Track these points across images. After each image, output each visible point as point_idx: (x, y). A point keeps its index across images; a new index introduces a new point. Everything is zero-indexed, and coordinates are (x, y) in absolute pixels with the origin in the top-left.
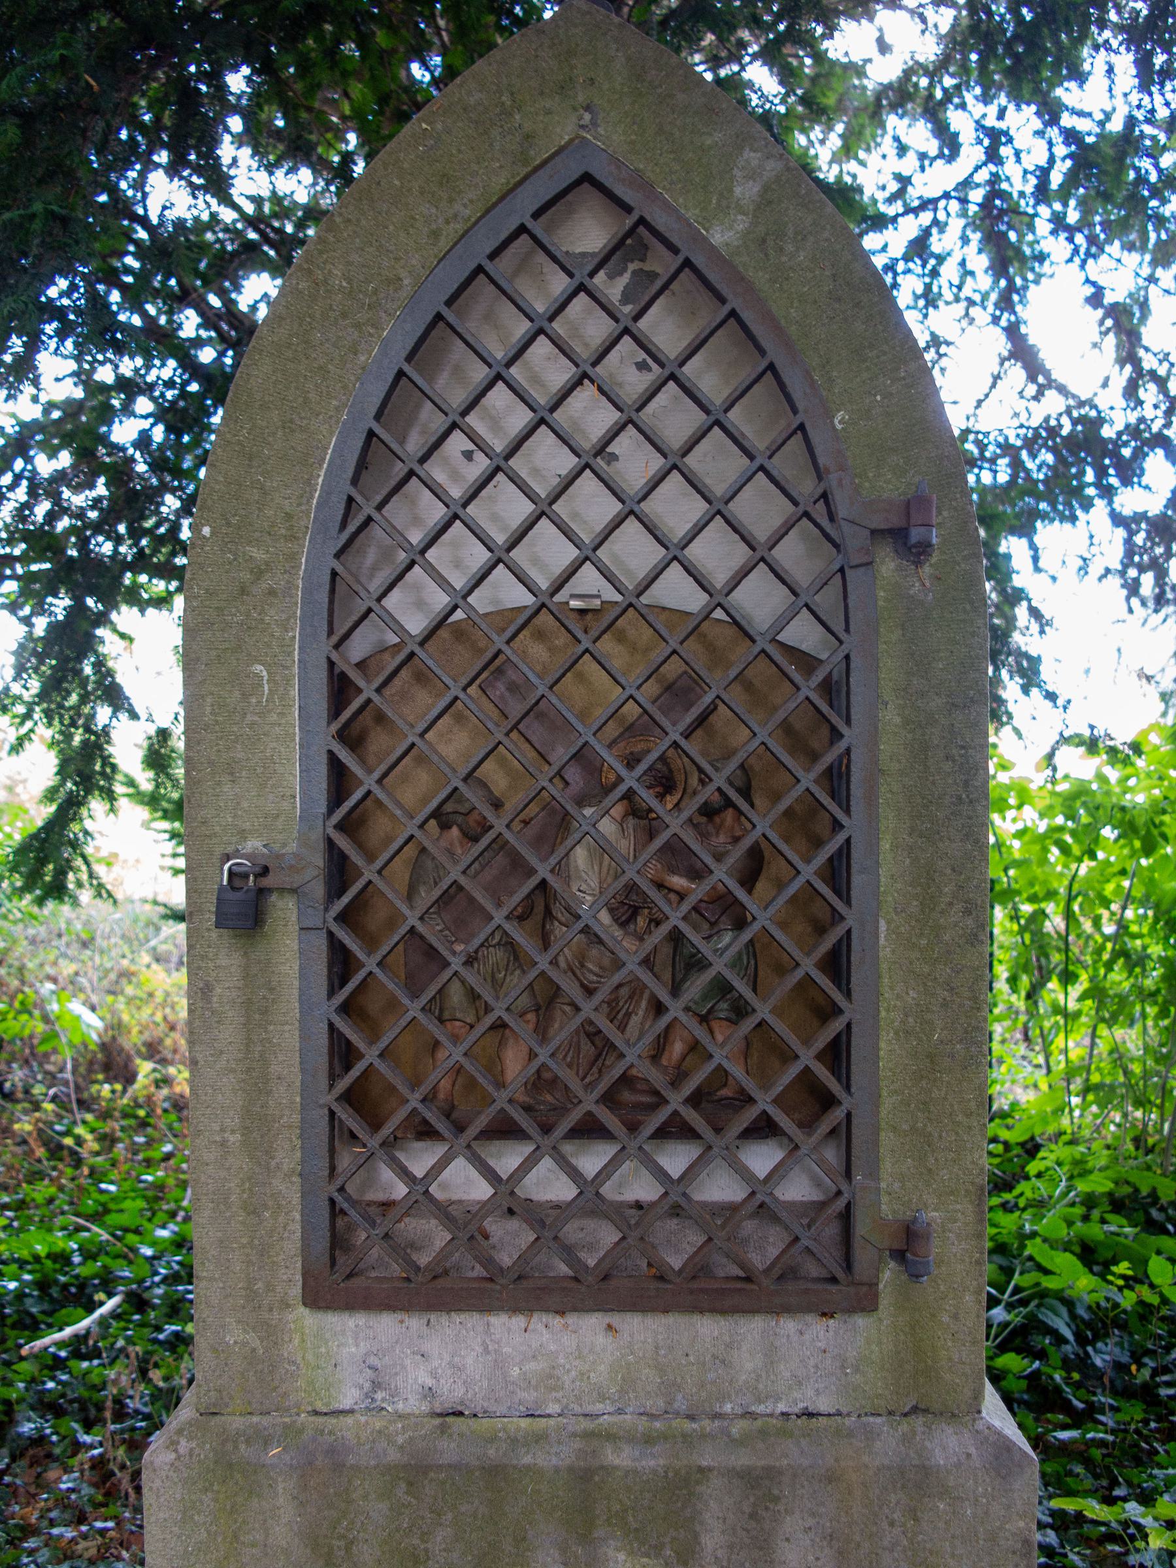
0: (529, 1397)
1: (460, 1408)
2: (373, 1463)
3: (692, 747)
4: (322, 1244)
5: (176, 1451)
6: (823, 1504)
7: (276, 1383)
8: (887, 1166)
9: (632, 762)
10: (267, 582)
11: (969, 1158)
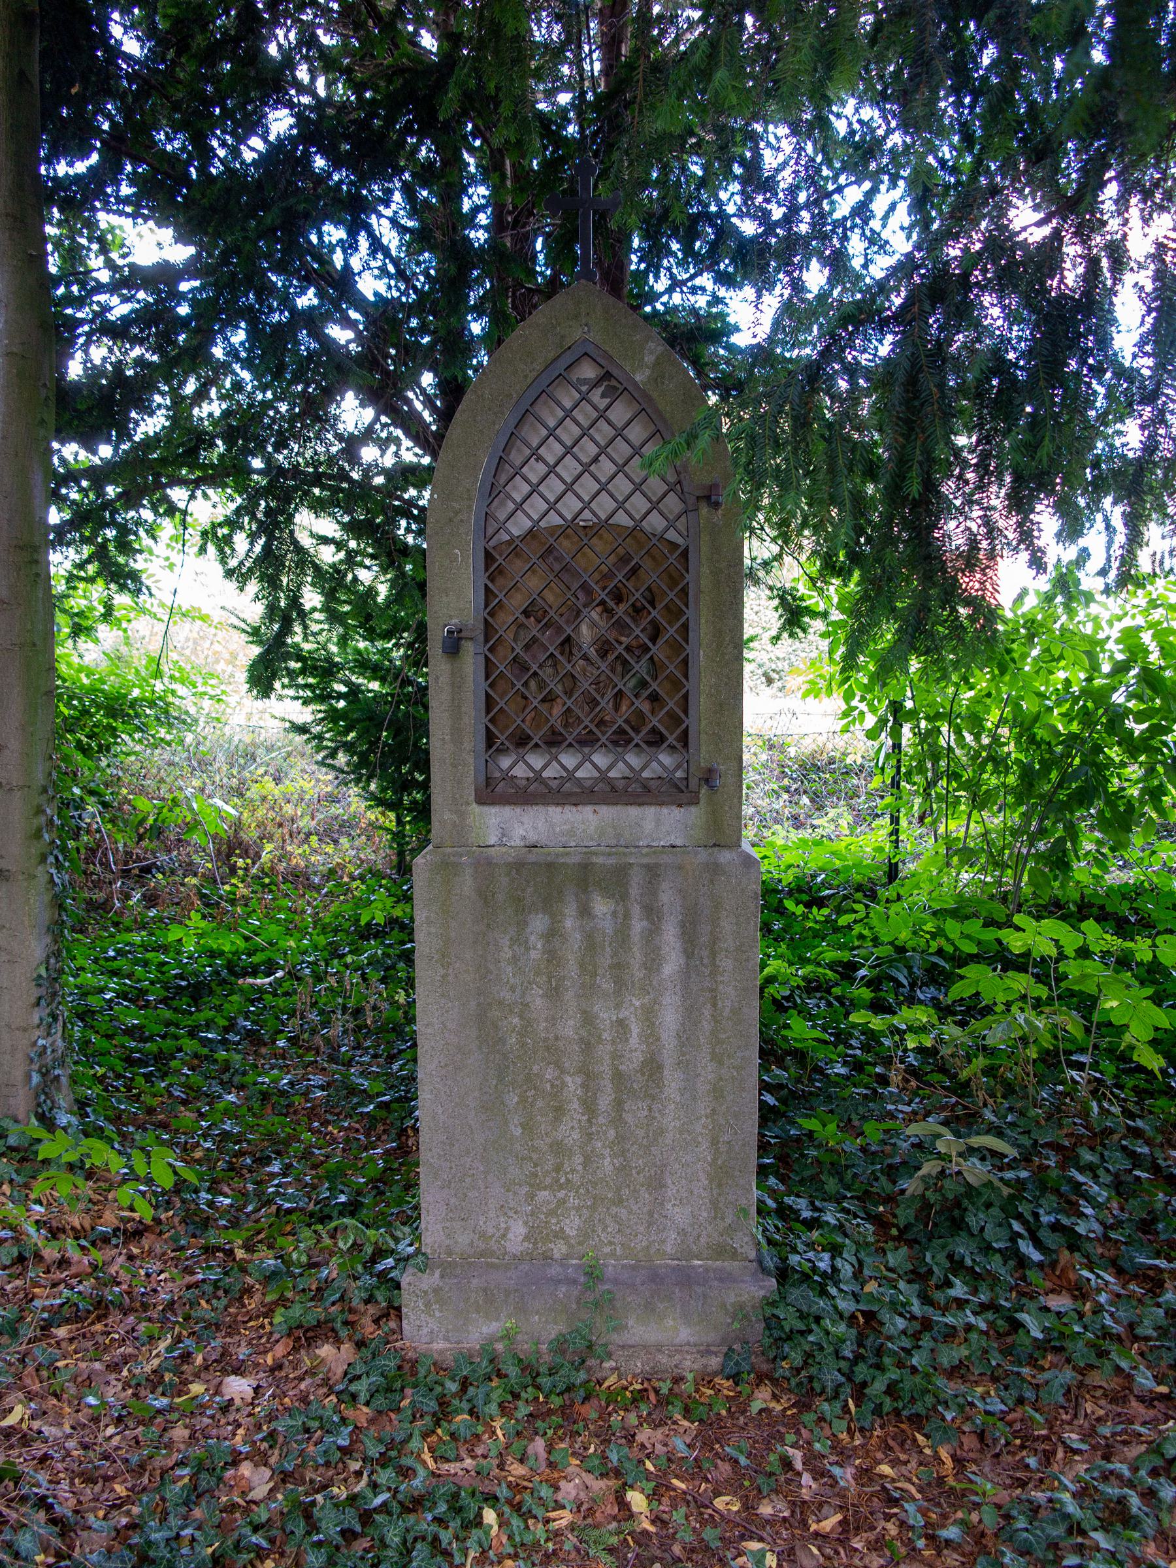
0: (563, 839)
3: (630, 585)
4: (482, 779)
9: (604, 589)
10: (460, 517)
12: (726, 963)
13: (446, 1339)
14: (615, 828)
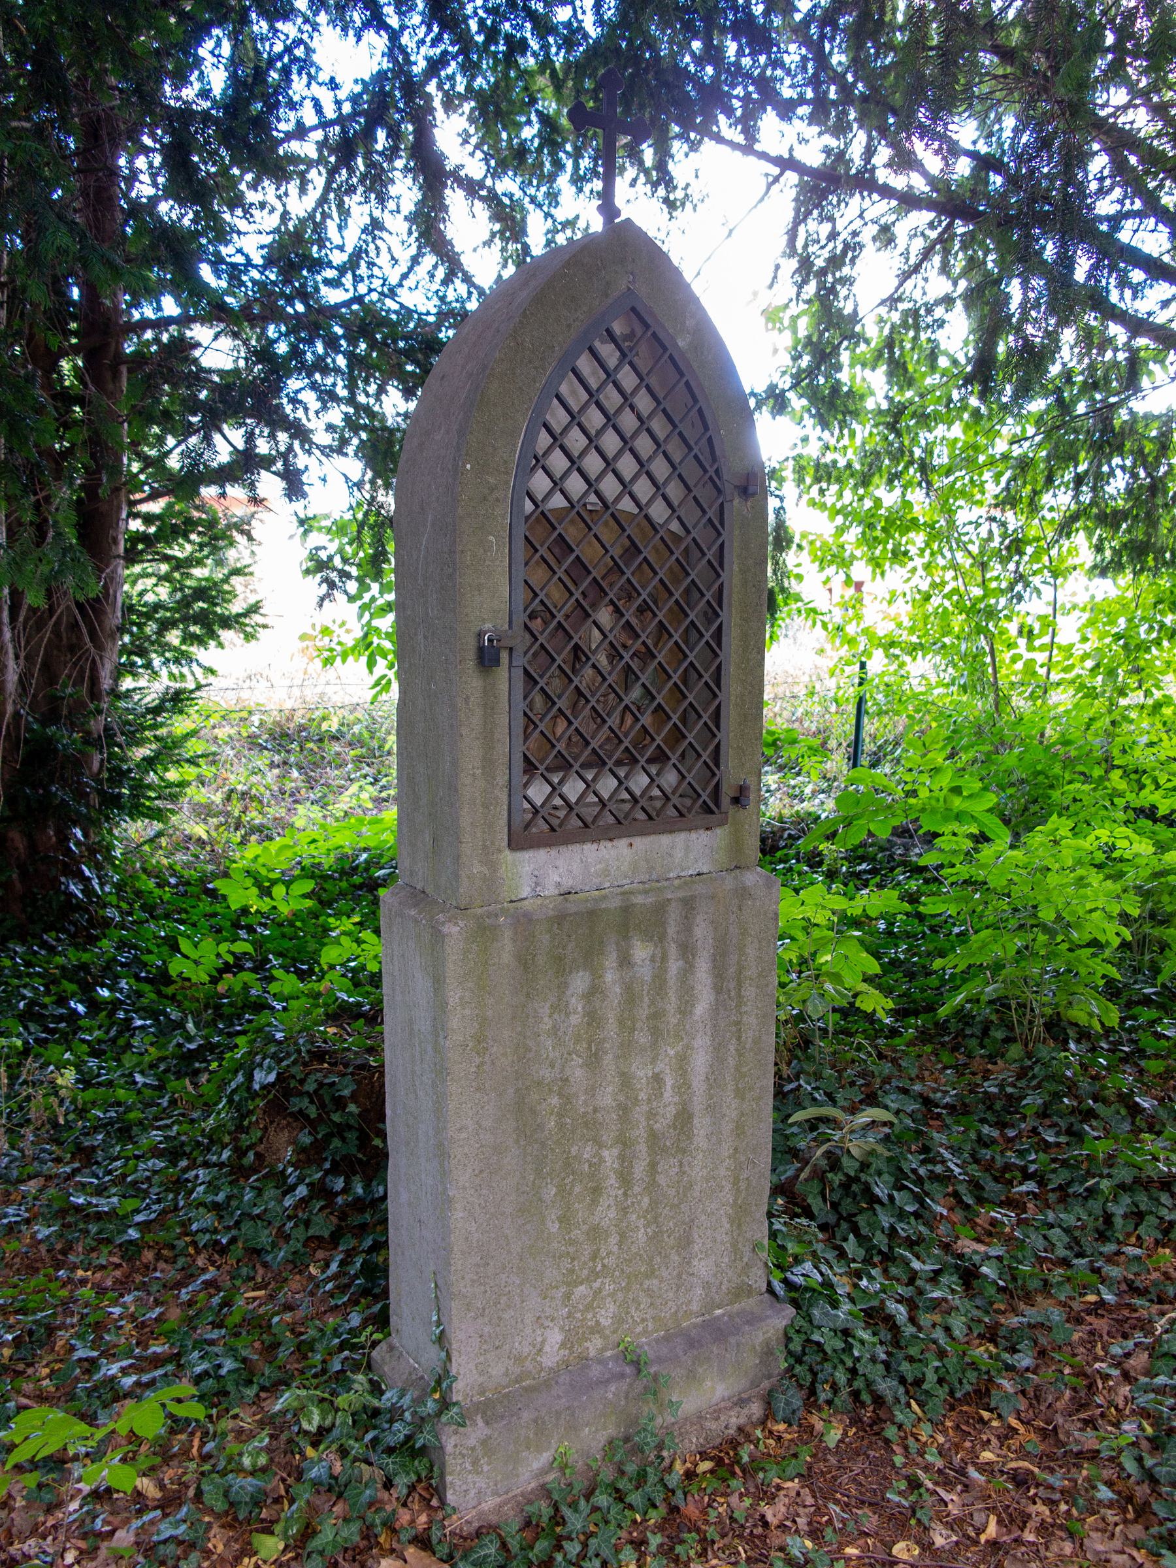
10: (496, 494)
12: (750, 992)
13: (496, 1493)
14: (647, 861)
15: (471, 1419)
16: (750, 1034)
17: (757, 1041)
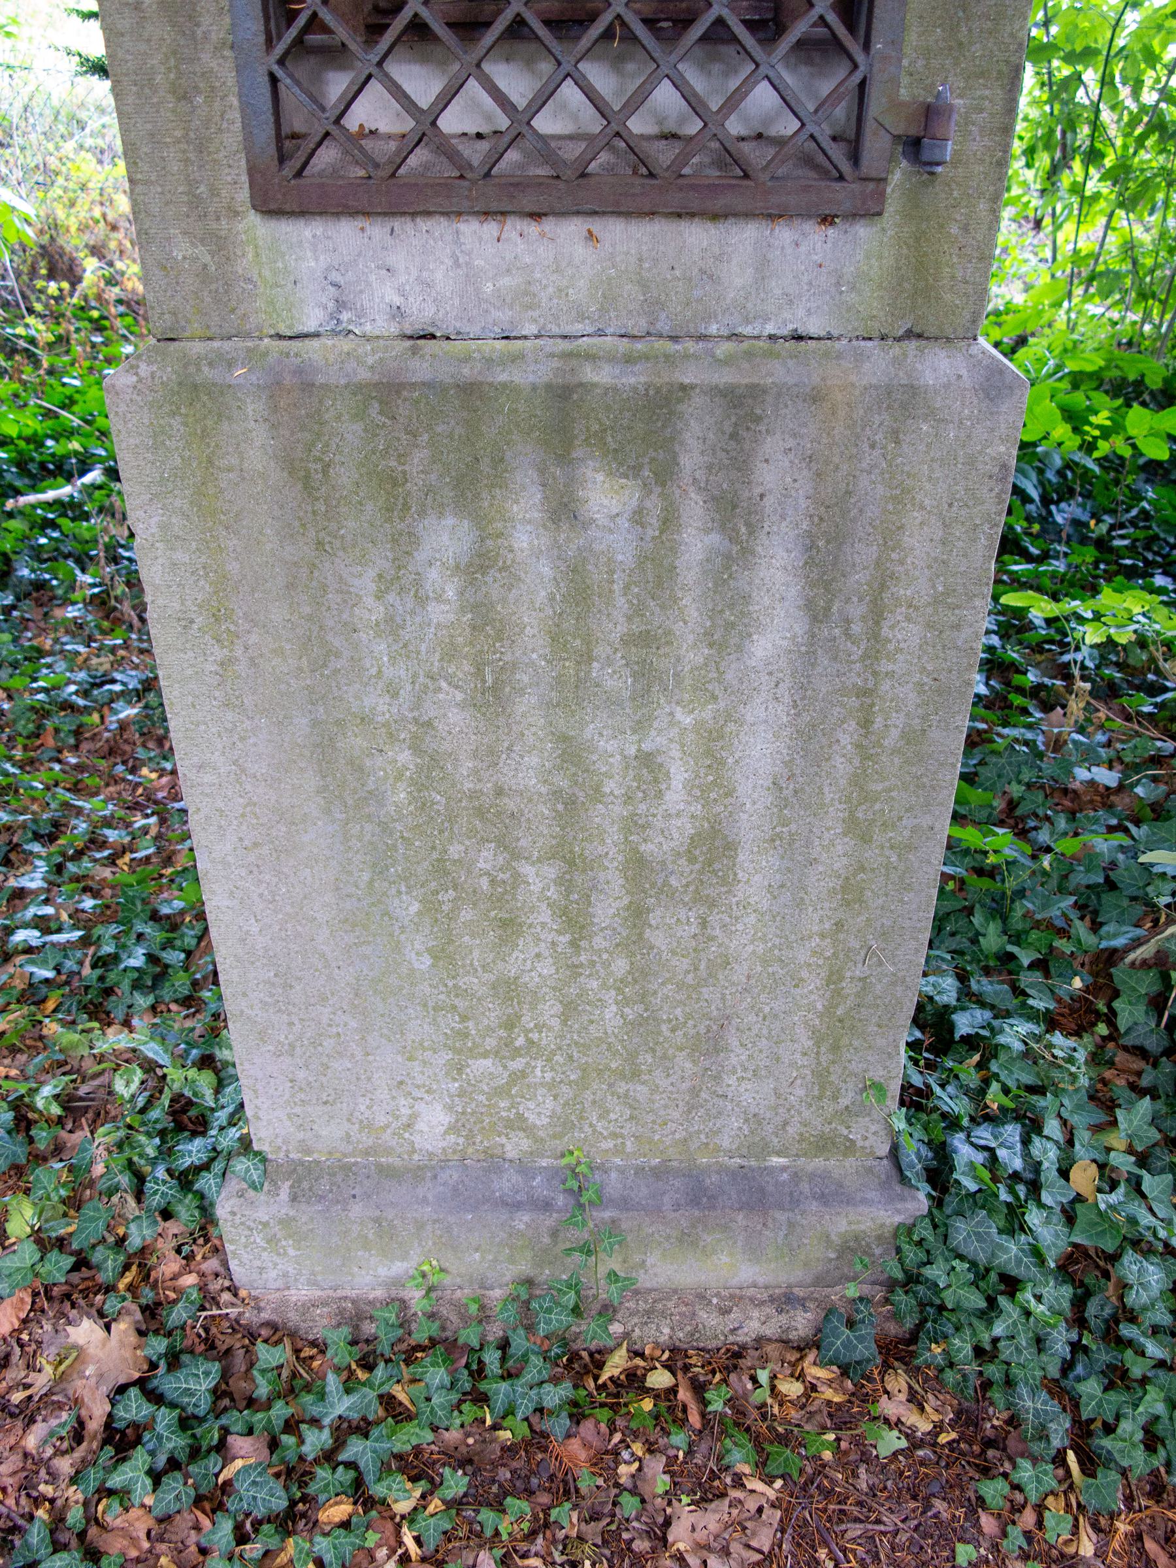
0: (502, 317)
1: (431, 330)
2: (343, 382)
4: (265, 134)
5: (137, 374)
6: (805, 425)
7: (233, 303)
8: (912, 38)
11: (1008, 29)
13: (313, 1283)
14: (644, 285)
15: (273, 1182)
16: (898, 720)
17: (912, 737)
